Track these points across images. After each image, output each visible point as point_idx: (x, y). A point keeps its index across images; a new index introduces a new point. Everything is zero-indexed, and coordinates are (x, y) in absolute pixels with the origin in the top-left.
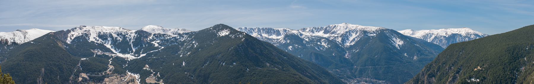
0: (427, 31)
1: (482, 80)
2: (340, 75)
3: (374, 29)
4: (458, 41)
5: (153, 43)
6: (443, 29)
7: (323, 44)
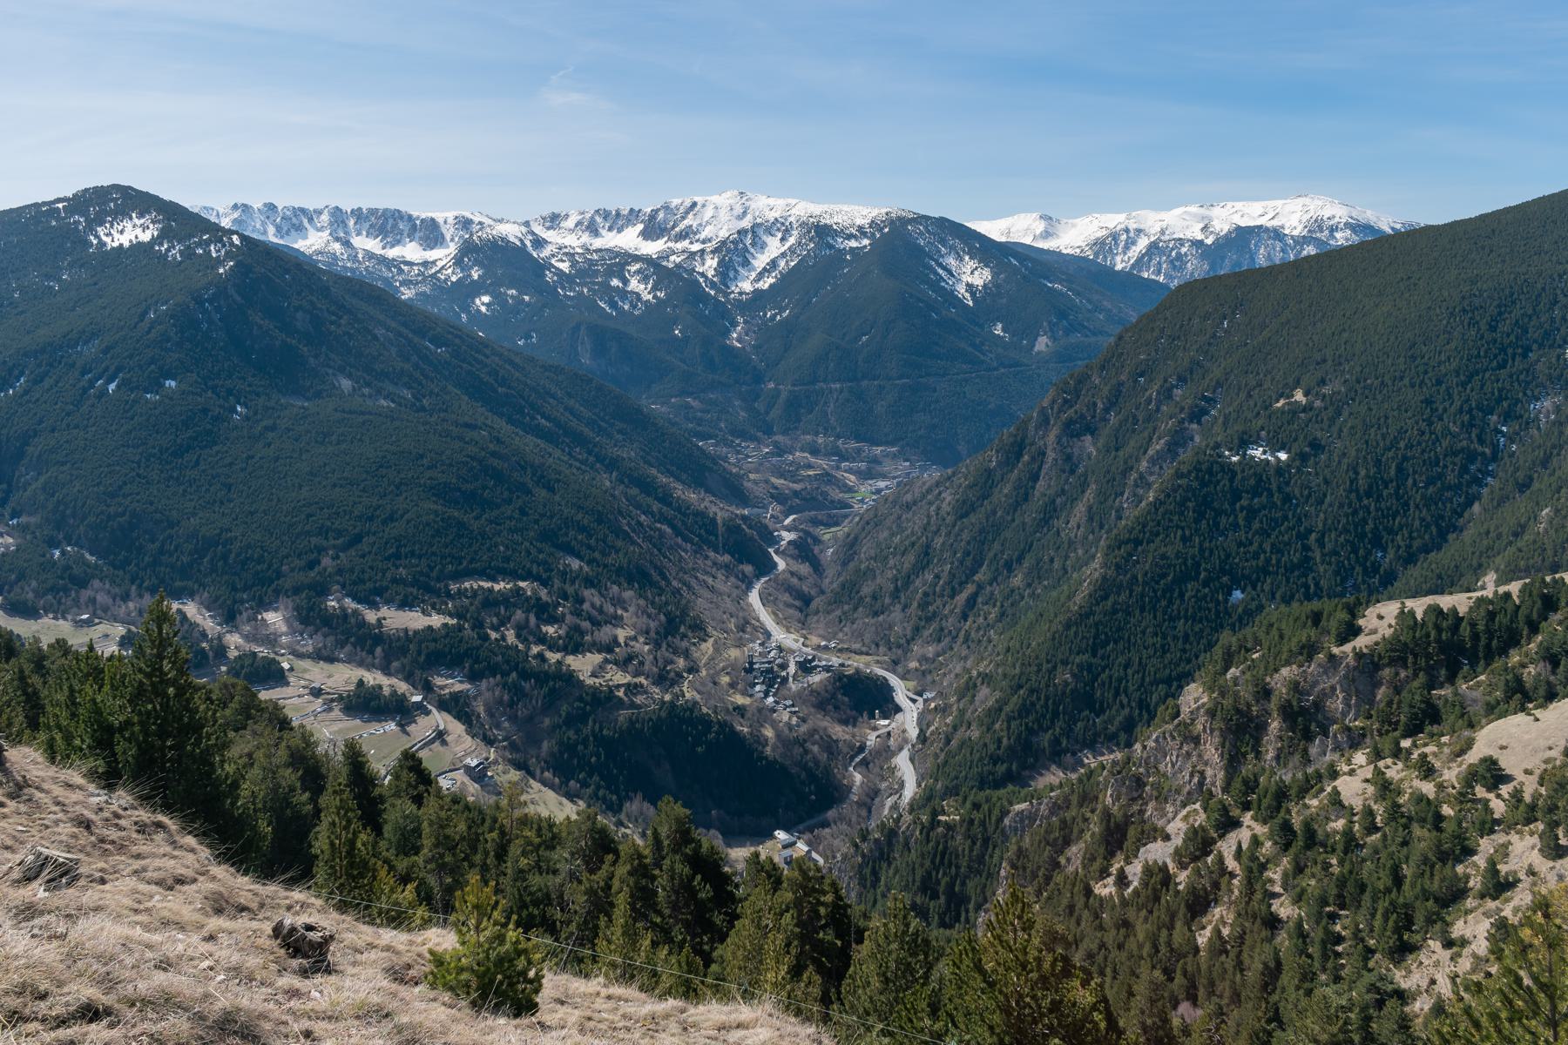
0: (1114, 221)
1: (1303, 457)
2: (700, 422)
4: (1261, 260)
6: (1194, 209)
7: (635, 285)
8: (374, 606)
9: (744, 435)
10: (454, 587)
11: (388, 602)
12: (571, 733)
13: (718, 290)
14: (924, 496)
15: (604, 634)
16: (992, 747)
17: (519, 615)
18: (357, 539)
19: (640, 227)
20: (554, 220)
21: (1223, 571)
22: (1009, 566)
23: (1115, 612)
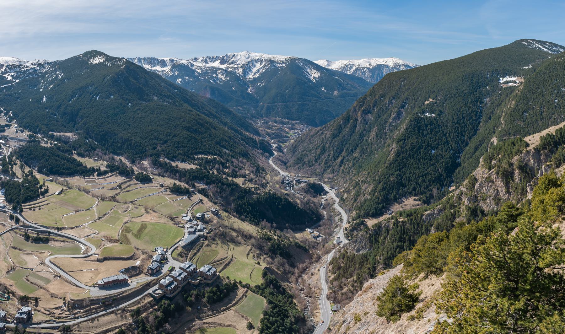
0: (346, 62)
3: (283, 58)
5: (6, 75)
6: (366, 60)
7: (220, 76)
8: (174, 161)
9: (255, 117)
10: (196, 157)
11: (178, 160)
12: (240, 201)
13: (243, 78)
14: (317, 133)
15: (243, 172)
16: (377, 200)
17: (217, 166)
18: (166, 142)
19: (219, 61)
20: (195, 59)
21: (428, 146)
22: (352, 151)
23: (403, 159)
